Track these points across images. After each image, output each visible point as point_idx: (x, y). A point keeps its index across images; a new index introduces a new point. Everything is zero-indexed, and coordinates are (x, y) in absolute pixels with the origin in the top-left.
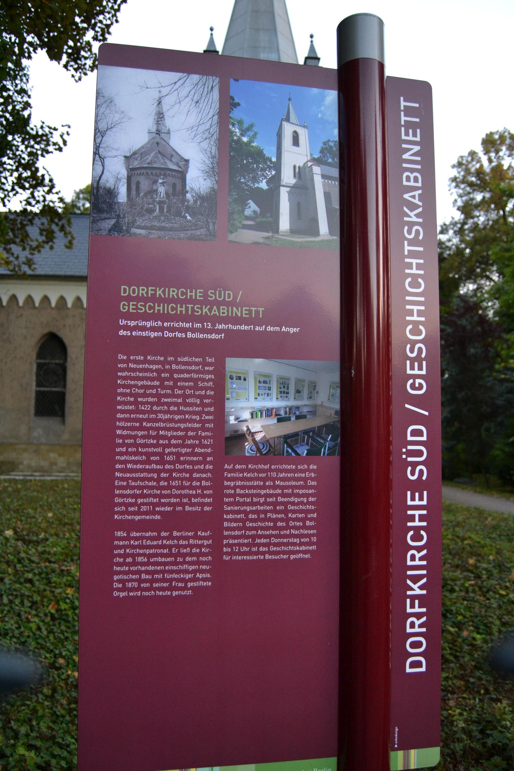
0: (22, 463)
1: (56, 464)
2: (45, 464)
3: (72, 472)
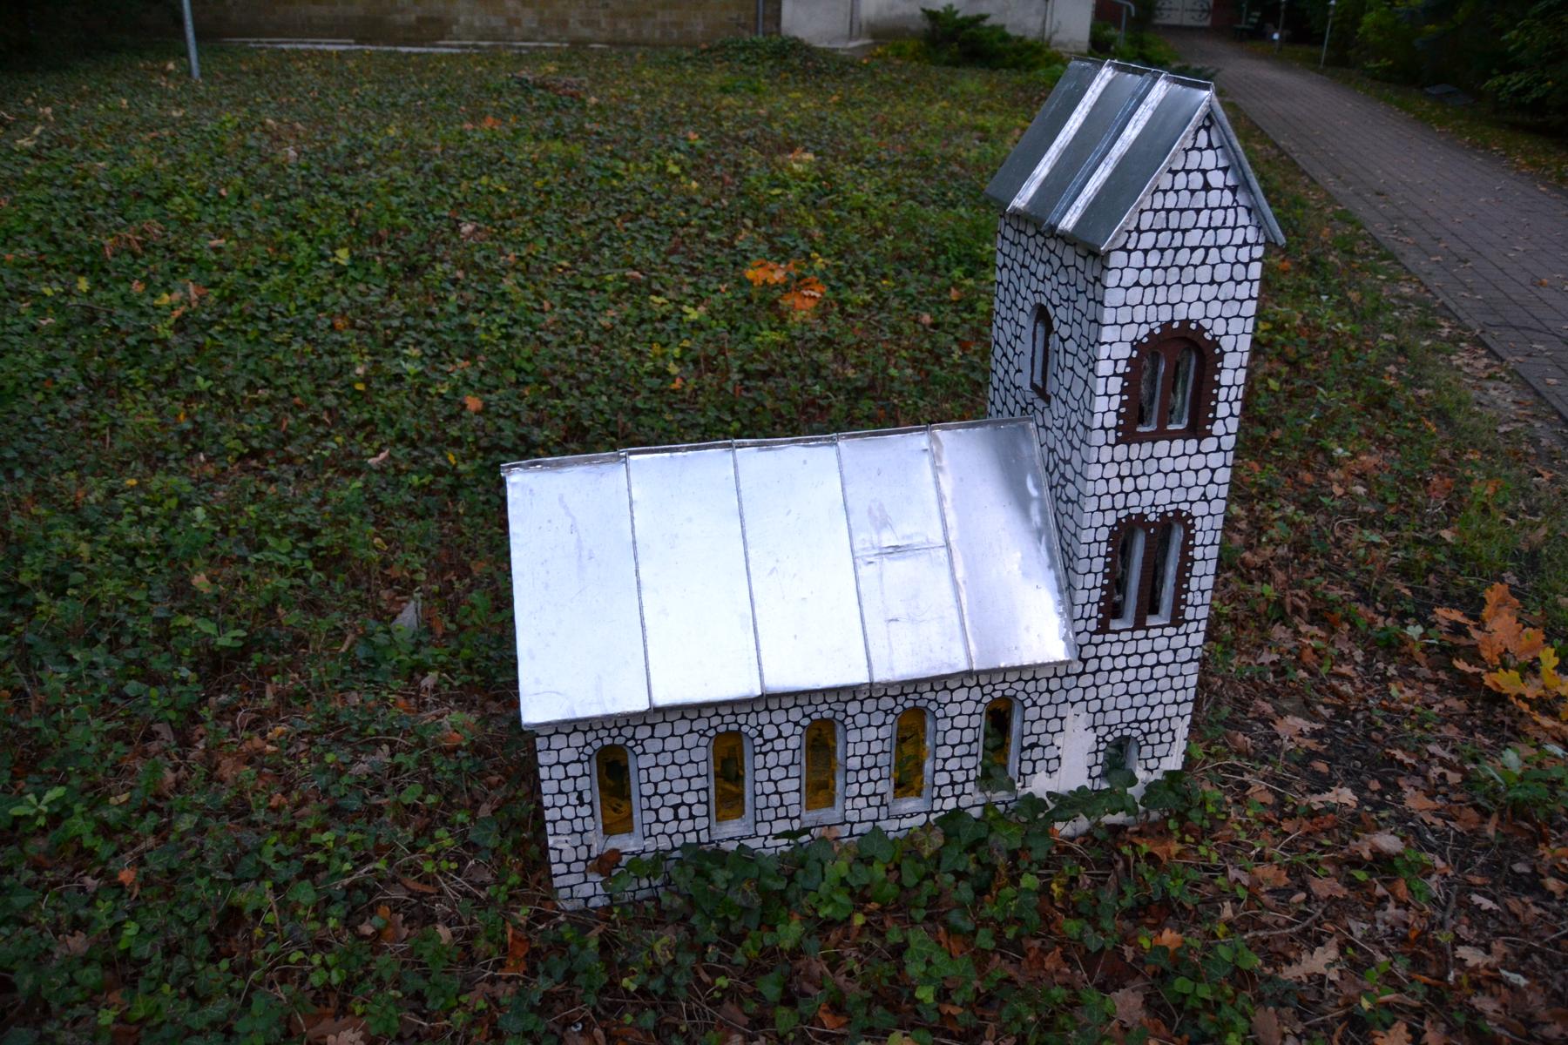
0: (456, 21)
1: (518, 22)
2: (498, 22)
3: (551, 39)
